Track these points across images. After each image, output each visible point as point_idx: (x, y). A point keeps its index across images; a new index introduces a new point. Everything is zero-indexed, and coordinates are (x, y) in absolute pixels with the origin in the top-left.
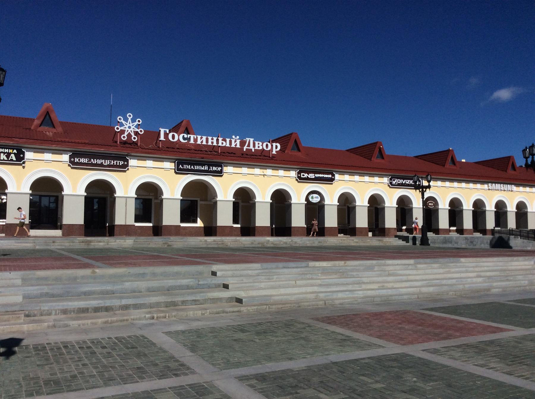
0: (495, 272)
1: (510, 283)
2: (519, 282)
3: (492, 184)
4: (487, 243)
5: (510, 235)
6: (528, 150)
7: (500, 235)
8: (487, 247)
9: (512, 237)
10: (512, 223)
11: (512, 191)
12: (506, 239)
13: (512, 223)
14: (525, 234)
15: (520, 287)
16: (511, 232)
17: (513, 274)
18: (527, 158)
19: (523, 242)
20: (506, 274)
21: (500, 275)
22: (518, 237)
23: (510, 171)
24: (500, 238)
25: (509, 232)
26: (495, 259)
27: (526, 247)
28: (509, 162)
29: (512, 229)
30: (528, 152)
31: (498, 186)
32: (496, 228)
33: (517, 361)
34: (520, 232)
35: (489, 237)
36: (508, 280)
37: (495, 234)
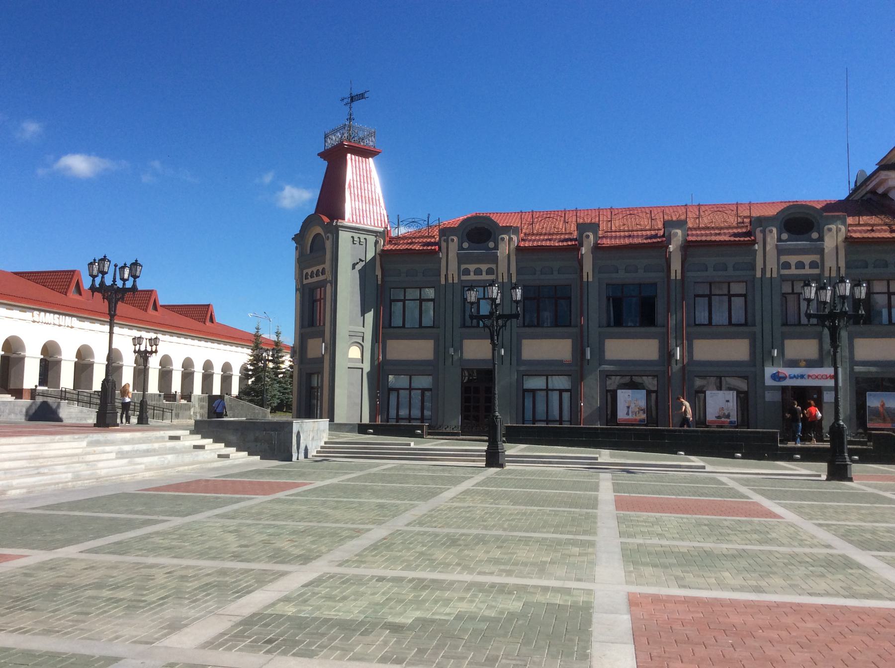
0: (10, 462)
1: (45, 477)
2: (57, 476)
3: (40, 313)
4: (21, 411)
5: (61, 399)
6: (97, 264)
7: (45, 399)
8: (21, 419)
9: (64, 403)
10: (67, 380)
11: (72, 327)
12: (54, 406)
13: (67, 380)
14: (86, 398)
15: (58, 483)
16: (63, 394)
17: (49, 463)
18: (94, 277)
19: (81, 412)
20: (38, 464)
21: (28, 465)
22: (75, 402)
23: (72, 294)
24: (45, 404)
25: (60, 395)
26: (23, 439)
27: (85, 420)
28: (71, 279)
29: (65, 390)
30: (97, 267)
31: (50, 317)
32: (39, 388)
33: (19, 605)
34: (90, 397)
35: (26, 402)
36: (39, 474)
37: (37, 397)
